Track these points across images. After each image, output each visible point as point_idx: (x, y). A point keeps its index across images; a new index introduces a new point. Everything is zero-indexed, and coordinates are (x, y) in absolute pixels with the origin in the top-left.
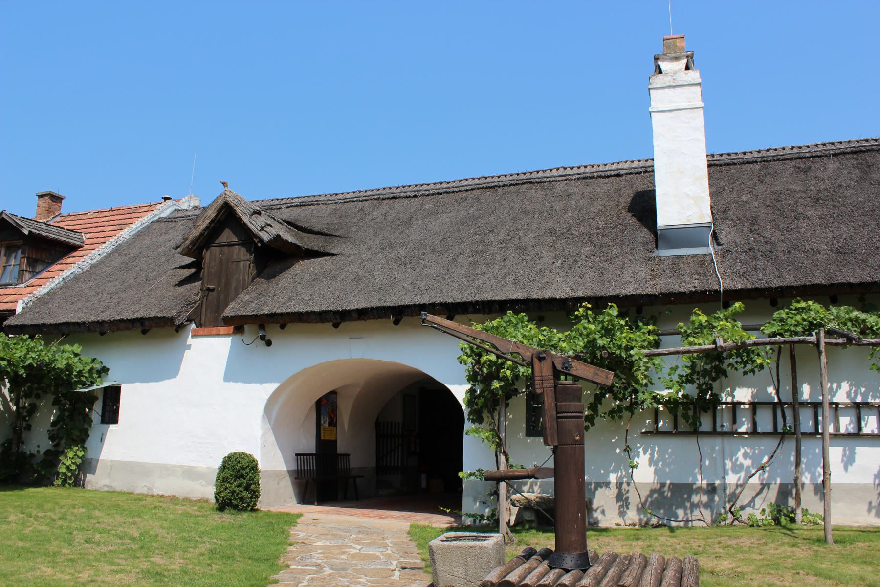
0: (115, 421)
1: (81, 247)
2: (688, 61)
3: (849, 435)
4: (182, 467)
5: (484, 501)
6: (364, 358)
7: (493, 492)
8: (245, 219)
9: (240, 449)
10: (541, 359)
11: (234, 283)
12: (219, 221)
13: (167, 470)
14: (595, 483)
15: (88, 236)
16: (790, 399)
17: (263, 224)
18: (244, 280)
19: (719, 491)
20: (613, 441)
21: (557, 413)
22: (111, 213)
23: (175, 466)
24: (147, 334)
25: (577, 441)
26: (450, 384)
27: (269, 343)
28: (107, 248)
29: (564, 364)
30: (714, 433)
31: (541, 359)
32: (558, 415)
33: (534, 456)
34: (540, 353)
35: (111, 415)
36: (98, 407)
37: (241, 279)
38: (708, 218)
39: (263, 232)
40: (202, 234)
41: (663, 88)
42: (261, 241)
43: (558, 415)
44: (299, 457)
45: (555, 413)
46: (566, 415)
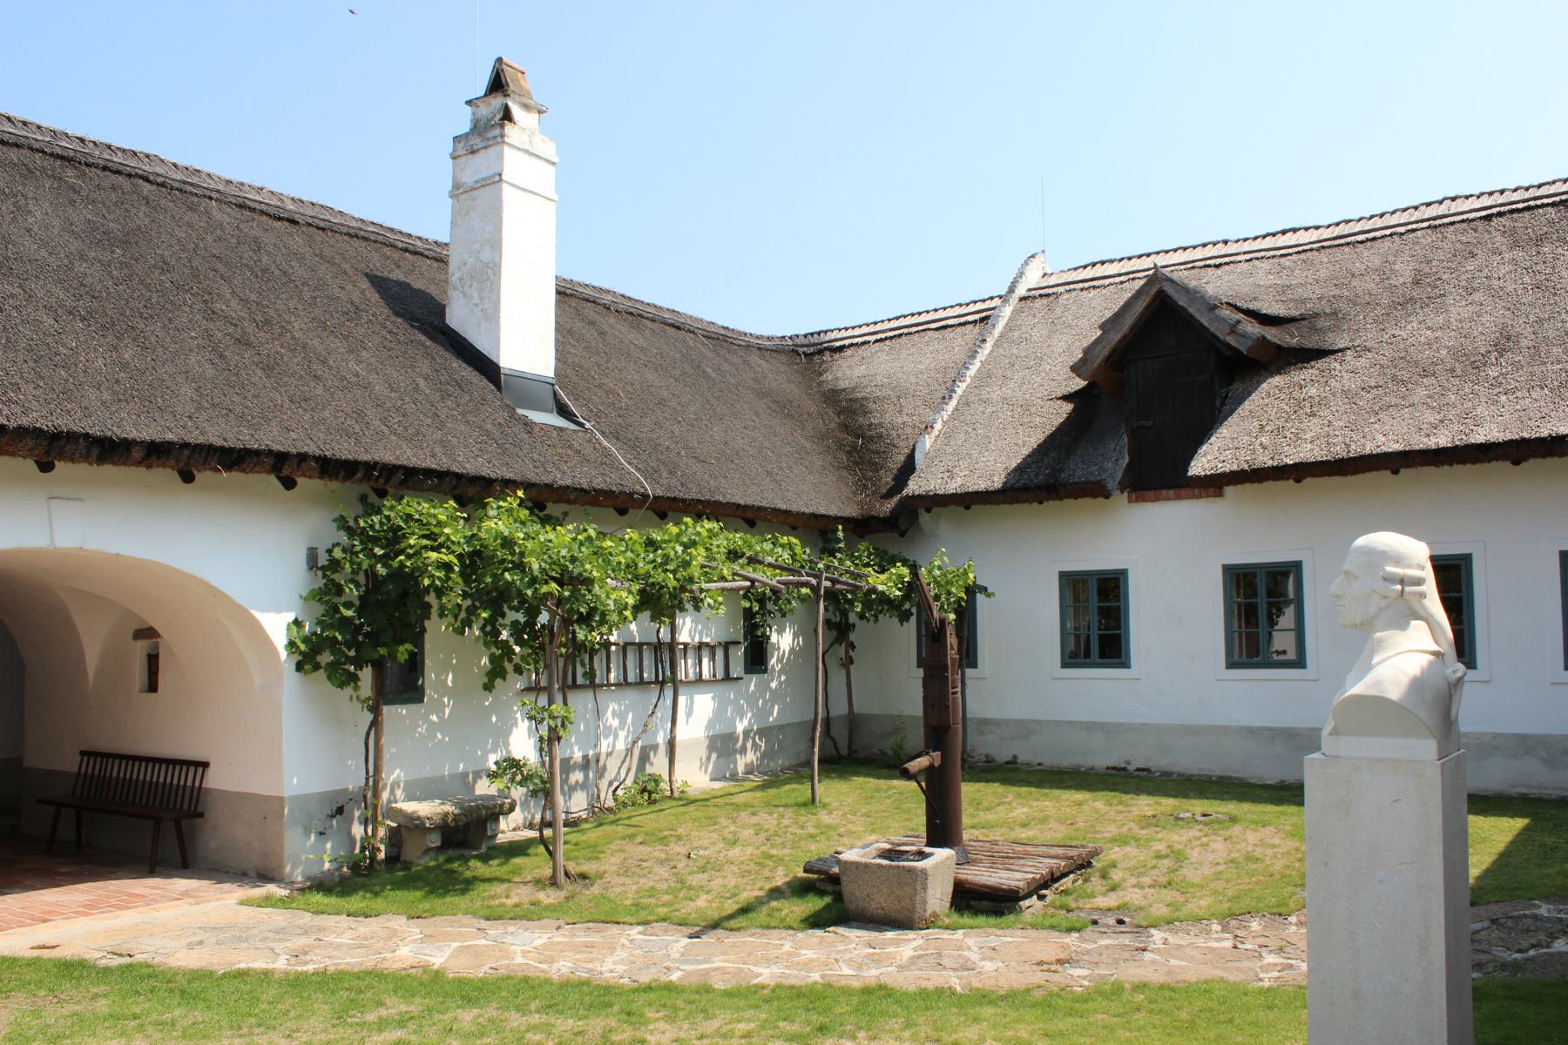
0: (974, 665)
3: (636, 684)
5: (322, 830)
6: (86, 546)
7: (334, 811)
14: (473, 772)
16: (668, 639)
19: (593, 764)
20: (487, 703)
26: (256, 609)
33: (409, 742)
38: (552, 374)
41: (519, 149)
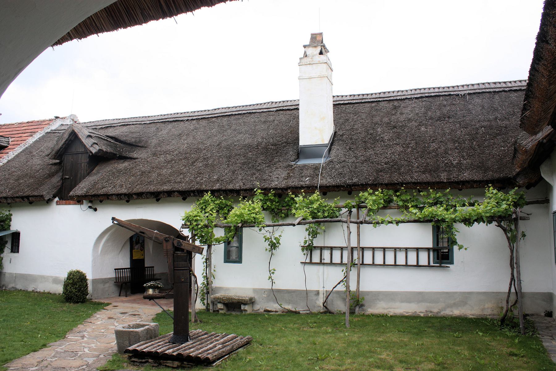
1: (7, 147)
2: (321, 49)
4: (52, 277)
8: (83, 140)
9: (74, 269)
10: (167, 241)
11: (79, 175)
12: (70, 140)
13: (43, 278)
15: (13, 139)
17: (92, 143)
18: (84, 173)
21: (174, 268)
22: (28, 124)
23: (48, 277)
24: (32, 204)
25: (183, 281)
27: (95, 210)
28: (18, 150)
29: (178, 243)
30: (321, 263)
31: (167, 241)
32: (175, 268)
34: (167, 238)
35: (15, 248)
36: (9, 245)
37: (83, 173)
39: (92, 148)
40: (61, 148)
42: (91, 152)
43: (175, 268)
44: (117, 270)
45: (173, 267)
46: (177, 268)
